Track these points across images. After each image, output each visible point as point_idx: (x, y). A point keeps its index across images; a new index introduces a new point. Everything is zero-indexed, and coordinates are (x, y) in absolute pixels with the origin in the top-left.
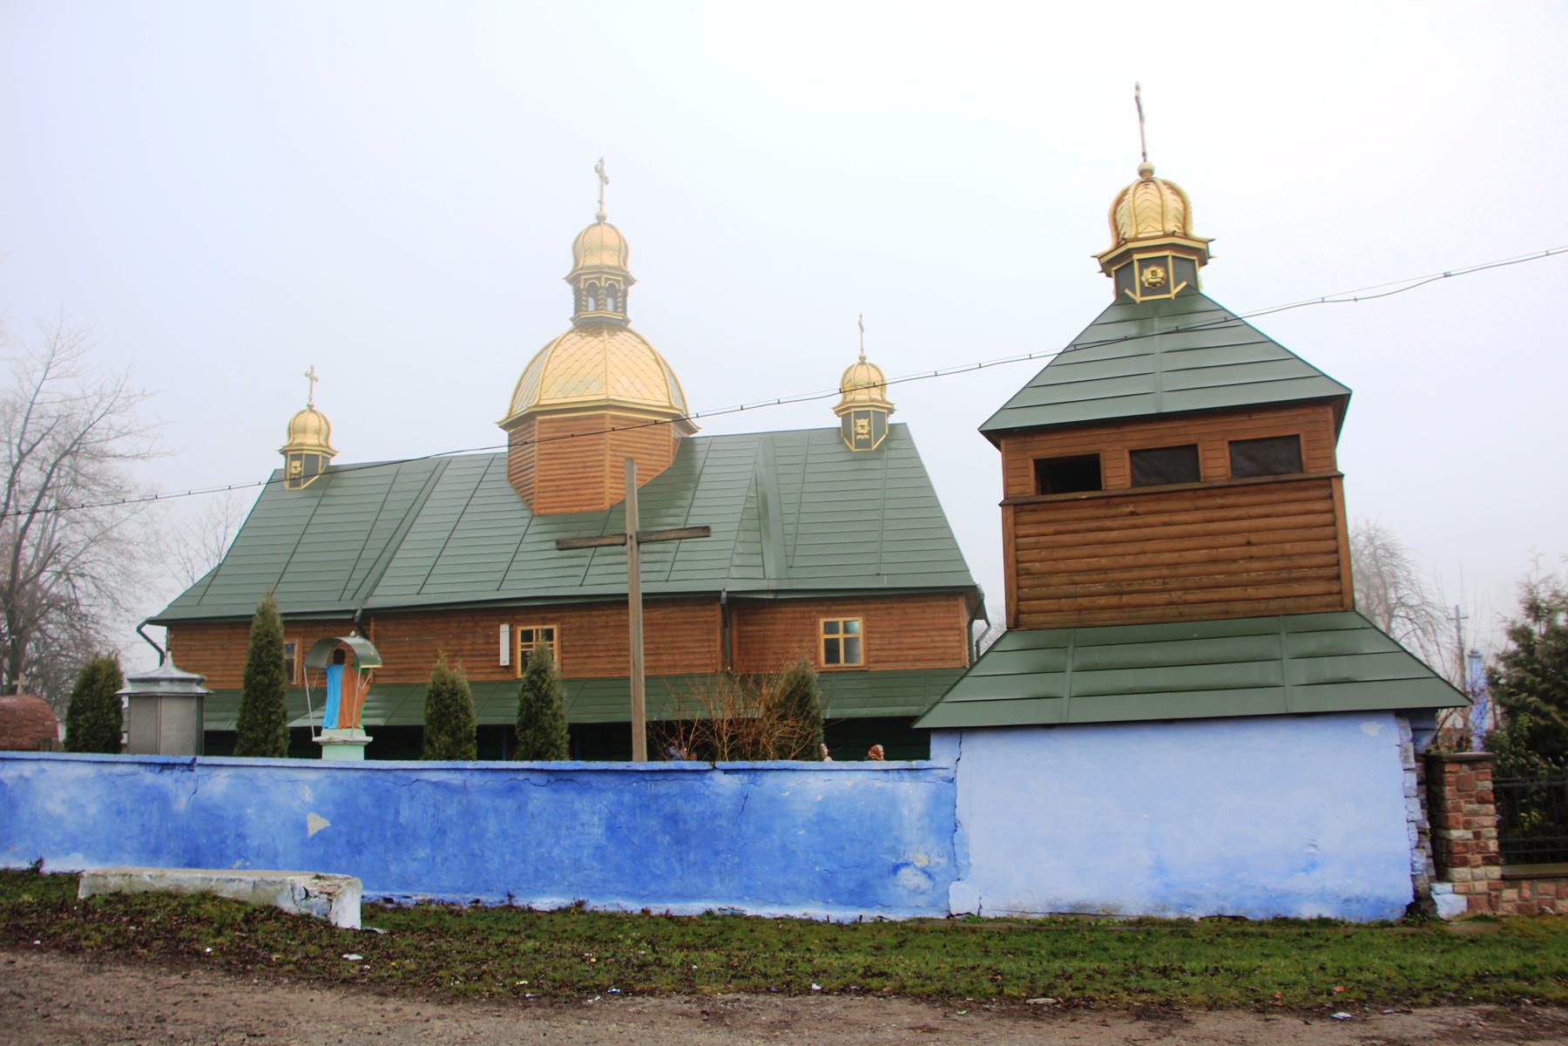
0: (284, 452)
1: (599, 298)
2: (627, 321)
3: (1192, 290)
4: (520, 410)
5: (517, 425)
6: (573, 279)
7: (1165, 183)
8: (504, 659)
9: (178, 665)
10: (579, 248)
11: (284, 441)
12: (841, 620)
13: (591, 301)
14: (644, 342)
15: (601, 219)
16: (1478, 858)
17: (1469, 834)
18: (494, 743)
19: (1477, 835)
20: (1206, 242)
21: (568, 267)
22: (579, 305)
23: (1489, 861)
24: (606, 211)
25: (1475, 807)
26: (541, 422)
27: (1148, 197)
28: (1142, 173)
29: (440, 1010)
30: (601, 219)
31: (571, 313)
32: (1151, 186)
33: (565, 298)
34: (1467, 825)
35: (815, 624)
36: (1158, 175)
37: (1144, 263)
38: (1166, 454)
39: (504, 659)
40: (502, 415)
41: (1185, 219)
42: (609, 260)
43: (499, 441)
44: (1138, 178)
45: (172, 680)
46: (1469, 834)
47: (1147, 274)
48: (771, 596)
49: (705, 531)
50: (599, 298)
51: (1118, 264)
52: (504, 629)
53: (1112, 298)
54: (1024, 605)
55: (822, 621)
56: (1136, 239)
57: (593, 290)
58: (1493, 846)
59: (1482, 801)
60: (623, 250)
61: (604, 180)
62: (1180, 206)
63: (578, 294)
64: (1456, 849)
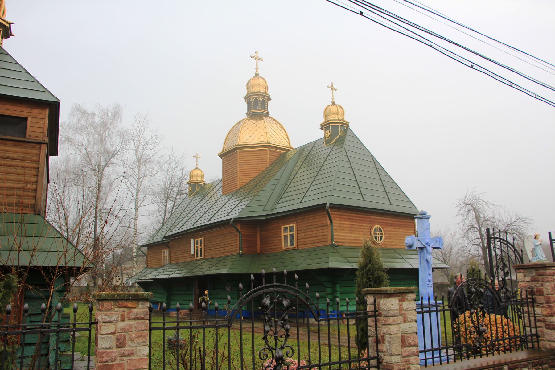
1: (257, 105)
2: (268, 114)
4: (230, 146)
5: (228, 155)
8: (192, 253)
10: (248, 86)
12: (288, 226)
14: (275, 120)
15: (257, 75)
18: (101, 179)
21: (245, 93)
22: (249, 109)
24: (259, 72)
26: (240, 152)
27: (334, 109)
28: (332, 102)
30: (257, 75)
31: (246, 111)
32: (335, 106)
33: (244, 106)
35: (281, 229)
39: (192, 253)
40: (220, 150)
42: (262, 90)
43: (320, 134)
44: (331, 103)
48: (264, 218)
50: (257, 105)
52: (192, 240)
54: (34, 179)
55: (283, 227)
57: (256, 102)
60: (267, 88)
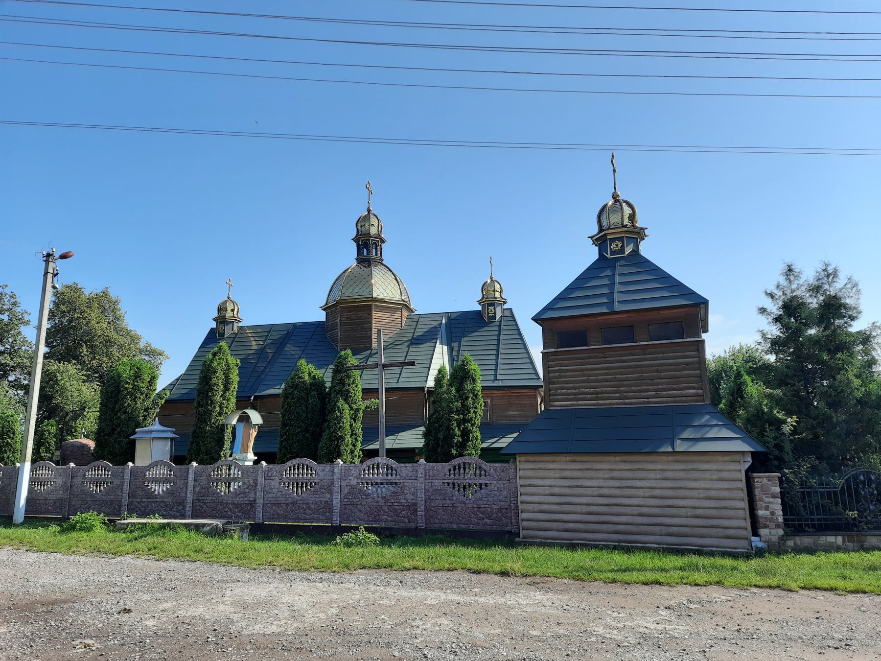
0: (215, 319)
3: (636, 252)
6: (356, 240)
7: (625, 201)
9: (161, 423)
11: (216, 315)
13: (365, 251)
16: (773, 525)
17: (768, 513)
19: (772, 513)
20: (643, 229)
22: (359, 252)
23: (778, 526)
25: (772, 500)
29: (320, 575)
31: (356, 256)
34: (767, 508)
36: (621, 198)
37: (612, 240)
38: (622, 329)
41: (632, 217)
45: (158, 431)
46: (768, 513)
47: (614, 245)
49: (413, 364)
51: (600, 241)
53: (597, 257)
56: (609, 229)
58: (781, 519)
59: (774, 497)
61: (370, 192)
62: (631, 212)
63: (358, 246)
64: (761, 520)
